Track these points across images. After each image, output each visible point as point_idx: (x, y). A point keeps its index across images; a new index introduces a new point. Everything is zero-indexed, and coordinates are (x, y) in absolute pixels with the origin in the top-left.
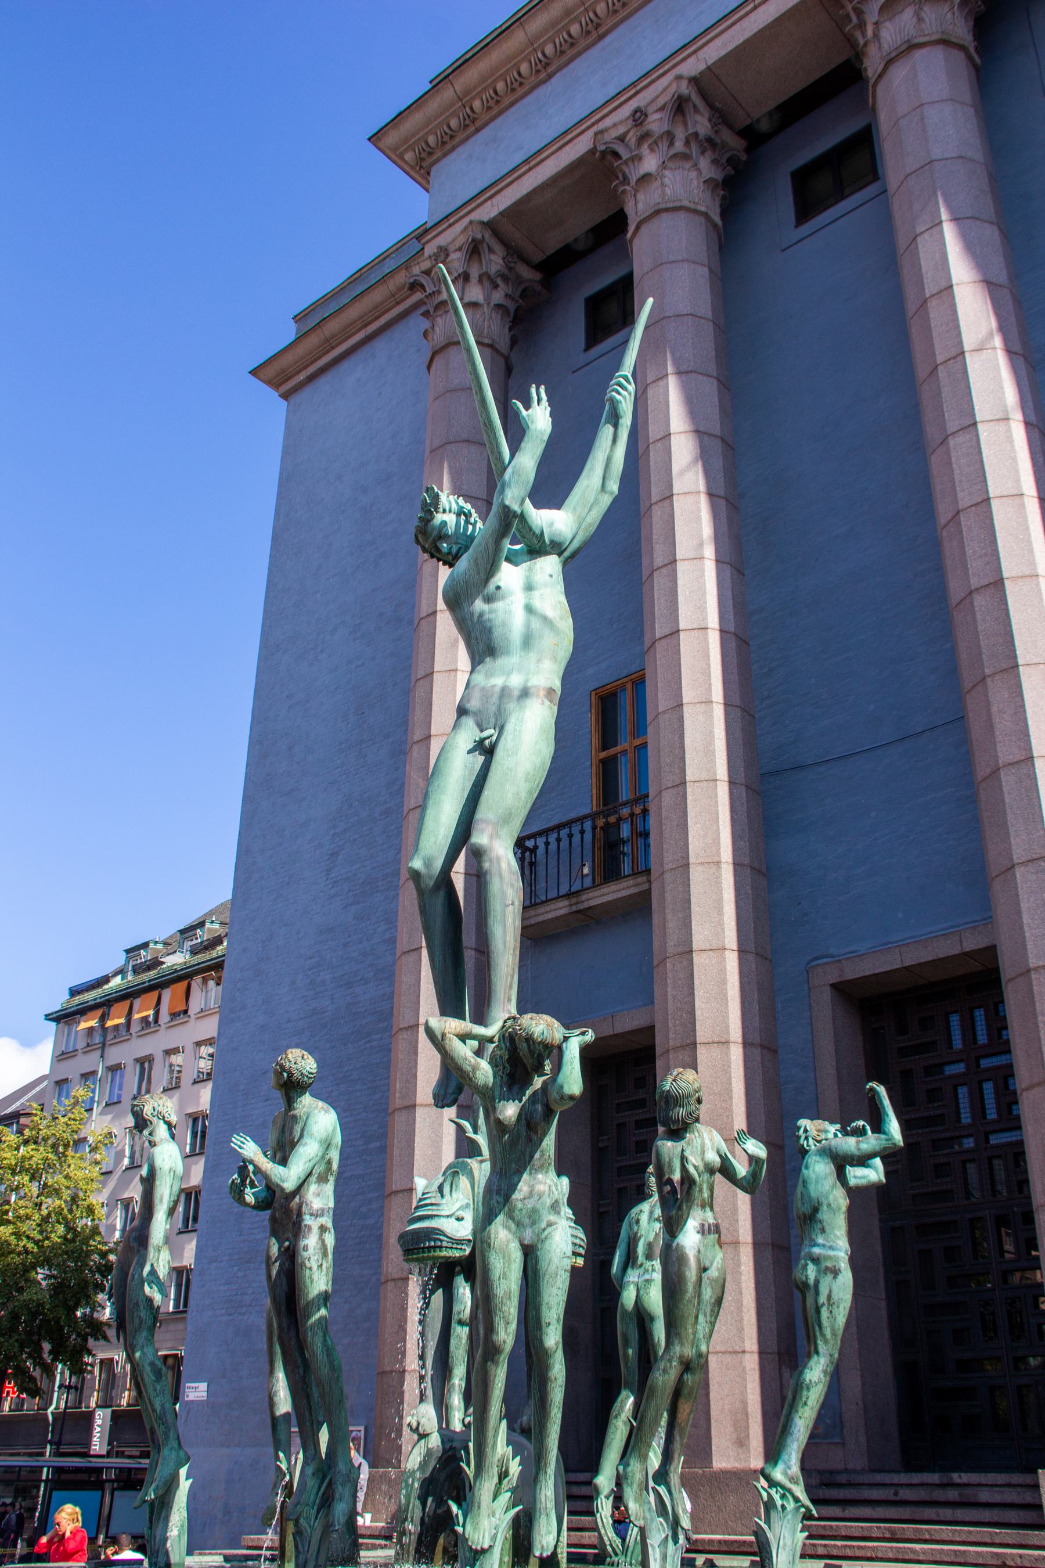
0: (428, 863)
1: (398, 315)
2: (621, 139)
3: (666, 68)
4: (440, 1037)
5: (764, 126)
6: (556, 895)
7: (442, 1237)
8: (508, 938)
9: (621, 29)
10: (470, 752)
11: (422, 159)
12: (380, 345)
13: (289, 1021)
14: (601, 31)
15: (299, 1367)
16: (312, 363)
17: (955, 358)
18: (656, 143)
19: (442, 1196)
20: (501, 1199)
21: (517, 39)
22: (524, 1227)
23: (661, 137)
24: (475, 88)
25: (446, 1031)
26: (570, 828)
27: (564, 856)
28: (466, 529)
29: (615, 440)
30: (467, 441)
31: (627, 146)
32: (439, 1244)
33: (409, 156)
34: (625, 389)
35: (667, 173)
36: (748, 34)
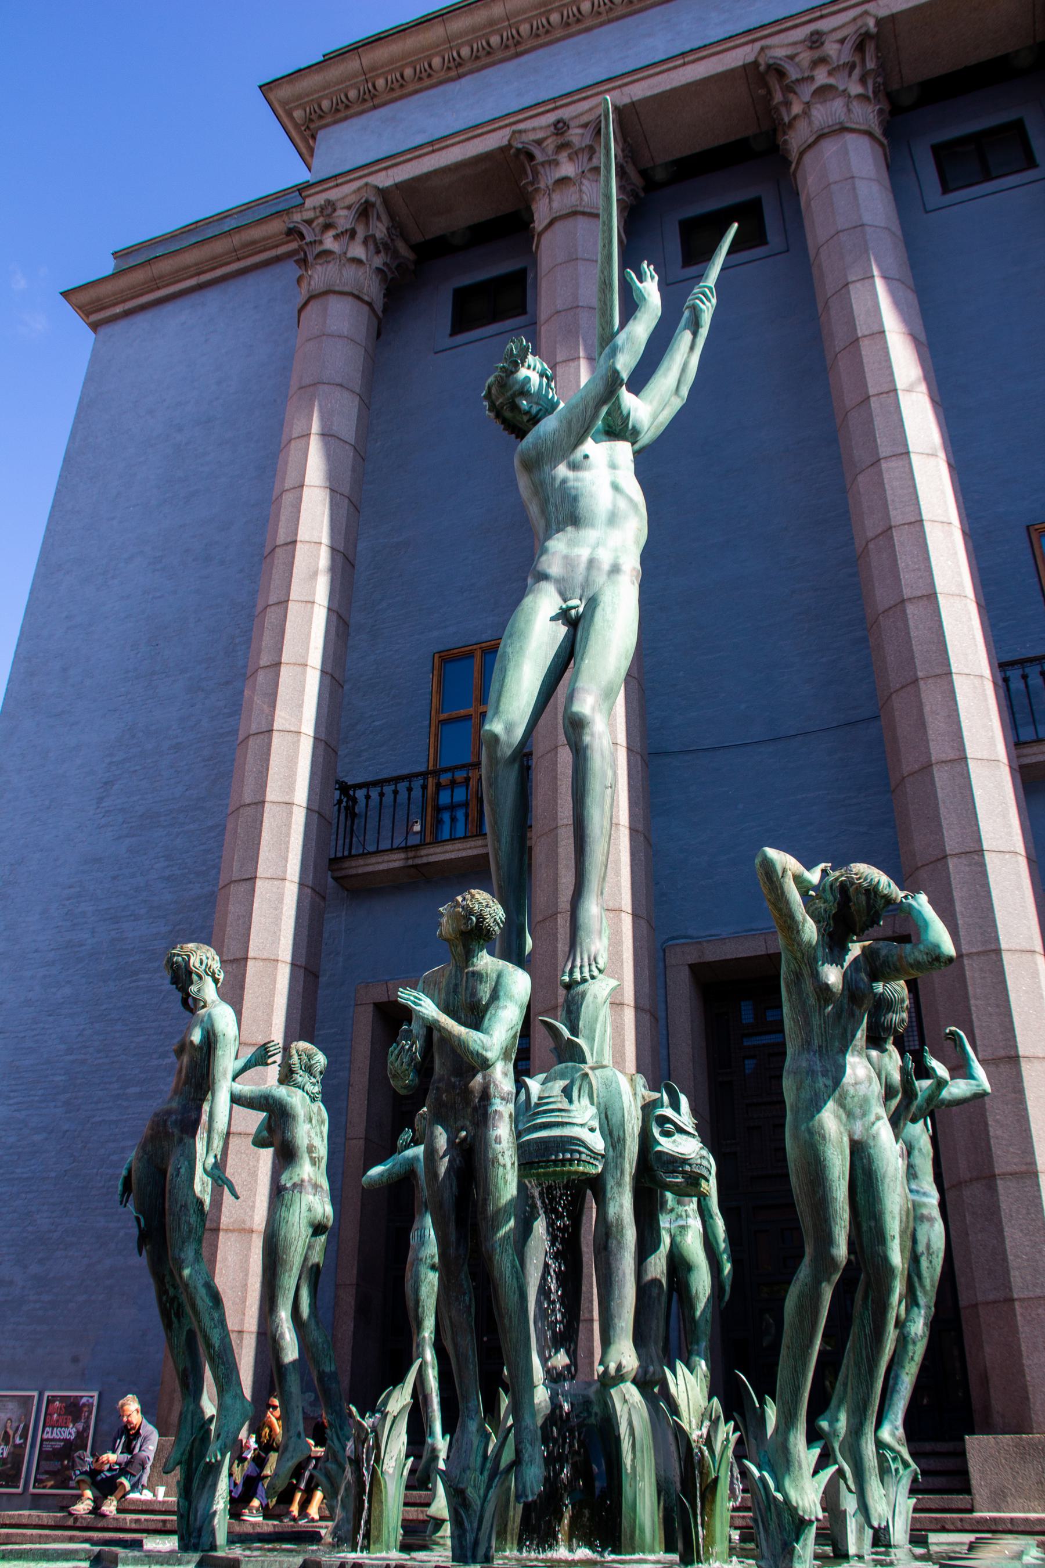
0: (509, 728)
1: (237, 271)
2: (539, 142)
3: (589, 93)
4: (780, 874)
5: (660, 175)
6: (389, 847)
7: (582, 1149)
8: (605, 823)
9: (540, 52)
10: (552, 619)
11: (311, 120)
12: (212, 296)
13: (36, 951)
14: (520, 49)
15: (465, 1294)
16: (133, 298)
17: (887, 393)
18: (576, 153)
19: (571, 1101)
20: (829, 1083)
21: (436, 33)
22: (854, 1118)
23: (582, 150)
24: (382, 67)
25: (788, 867)
26: (410, 782)
27: (387, 812)
28: (547, 393)
29: (692, 348)
30: (341, 385)
31: (543, 150)
32: (577, 1156)
33: (298, 114)
34: (709, 300)
35: (585, 182)
36: (676, 84)
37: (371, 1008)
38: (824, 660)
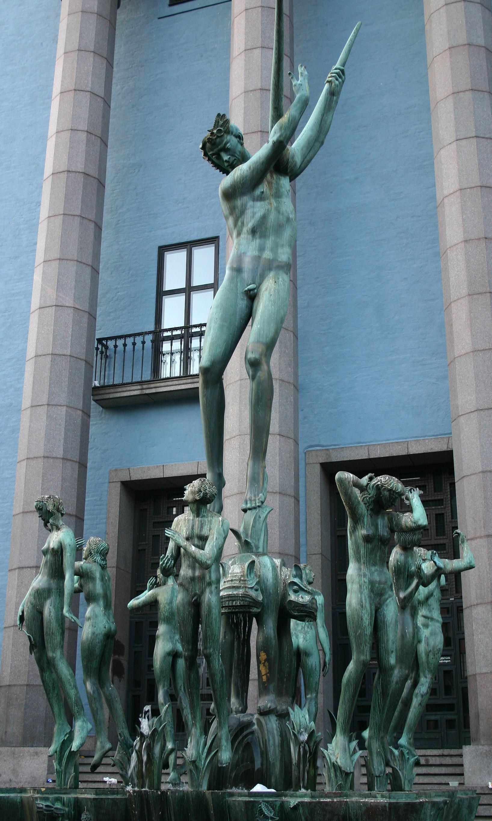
37: (119, 485)
38: (415, 266)
